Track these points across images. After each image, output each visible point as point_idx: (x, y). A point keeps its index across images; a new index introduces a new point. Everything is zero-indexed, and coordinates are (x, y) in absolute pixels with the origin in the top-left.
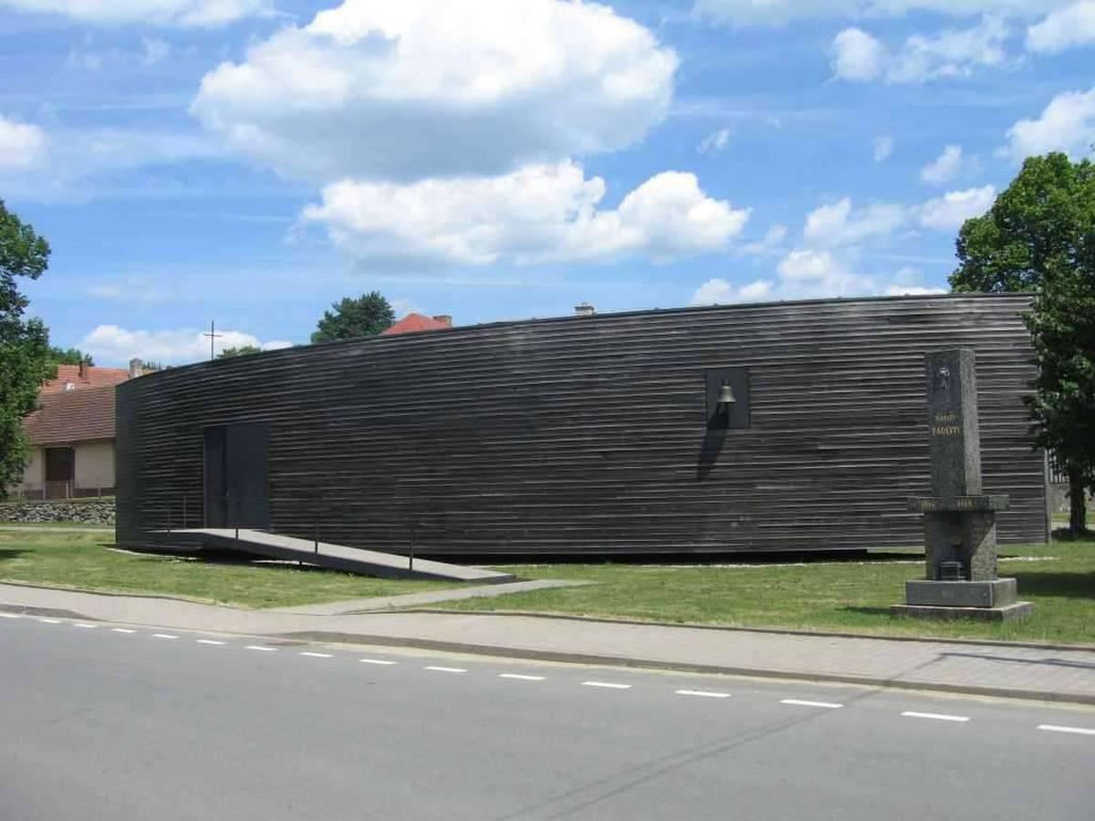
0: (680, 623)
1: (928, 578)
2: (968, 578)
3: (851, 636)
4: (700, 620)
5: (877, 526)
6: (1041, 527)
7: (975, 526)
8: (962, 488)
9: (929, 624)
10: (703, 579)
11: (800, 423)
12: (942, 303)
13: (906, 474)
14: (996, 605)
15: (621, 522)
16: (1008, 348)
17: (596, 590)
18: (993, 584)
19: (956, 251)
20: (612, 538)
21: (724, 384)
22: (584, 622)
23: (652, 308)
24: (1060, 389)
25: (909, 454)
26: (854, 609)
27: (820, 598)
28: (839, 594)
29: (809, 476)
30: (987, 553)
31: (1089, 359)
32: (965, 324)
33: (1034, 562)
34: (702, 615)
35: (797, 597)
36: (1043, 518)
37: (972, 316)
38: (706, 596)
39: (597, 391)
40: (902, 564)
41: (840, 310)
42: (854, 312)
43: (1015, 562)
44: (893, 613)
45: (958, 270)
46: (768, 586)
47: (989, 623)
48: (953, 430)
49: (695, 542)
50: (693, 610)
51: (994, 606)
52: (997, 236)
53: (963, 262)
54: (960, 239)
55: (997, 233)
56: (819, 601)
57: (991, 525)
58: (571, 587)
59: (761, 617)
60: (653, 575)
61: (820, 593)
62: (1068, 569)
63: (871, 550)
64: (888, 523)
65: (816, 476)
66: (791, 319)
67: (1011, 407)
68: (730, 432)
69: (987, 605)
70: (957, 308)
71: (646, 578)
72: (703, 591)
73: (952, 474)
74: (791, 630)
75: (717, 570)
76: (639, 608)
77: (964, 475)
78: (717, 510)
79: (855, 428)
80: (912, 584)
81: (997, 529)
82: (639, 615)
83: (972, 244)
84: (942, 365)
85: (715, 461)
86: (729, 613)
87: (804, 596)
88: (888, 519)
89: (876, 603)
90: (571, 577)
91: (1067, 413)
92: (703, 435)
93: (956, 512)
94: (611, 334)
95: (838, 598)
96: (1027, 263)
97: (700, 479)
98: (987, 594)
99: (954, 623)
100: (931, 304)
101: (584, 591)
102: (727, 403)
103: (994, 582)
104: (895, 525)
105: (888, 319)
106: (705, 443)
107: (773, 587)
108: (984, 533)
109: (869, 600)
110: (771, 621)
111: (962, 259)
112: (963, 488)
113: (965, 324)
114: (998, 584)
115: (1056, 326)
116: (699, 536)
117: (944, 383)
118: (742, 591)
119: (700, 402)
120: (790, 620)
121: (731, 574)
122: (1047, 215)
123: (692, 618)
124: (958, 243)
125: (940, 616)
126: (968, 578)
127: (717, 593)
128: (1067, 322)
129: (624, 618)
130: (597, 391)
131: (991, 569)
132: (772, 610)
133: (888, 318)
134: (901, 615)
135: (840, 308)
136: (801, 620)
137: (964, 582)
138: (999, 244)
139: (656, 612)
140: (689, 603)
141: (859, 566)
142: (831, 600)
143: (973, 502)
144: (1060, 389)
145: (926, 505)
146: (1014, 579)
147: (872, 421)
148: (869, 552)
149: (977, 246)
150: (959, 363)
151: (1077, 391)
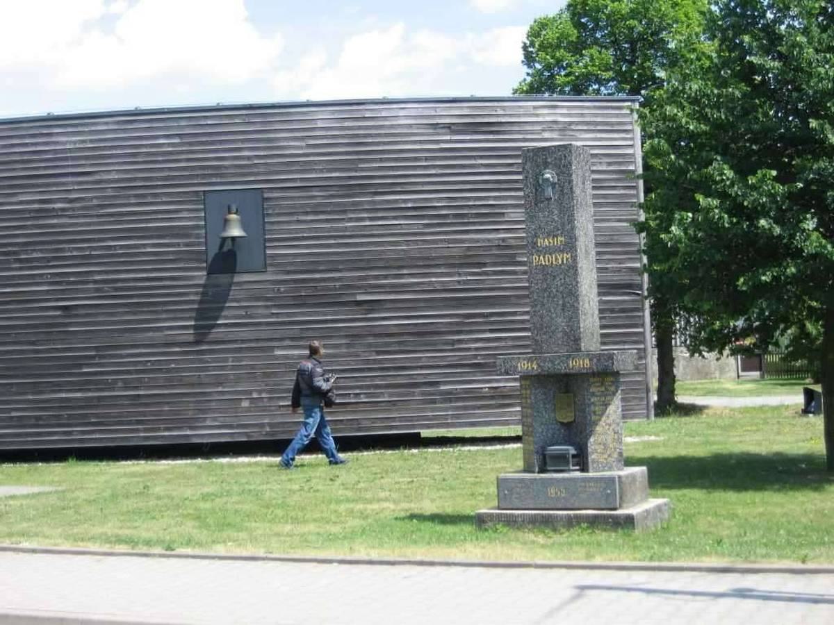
0: (169, 550)
1: (528, 469)
2: (584, 469)
3: (432, 564)
4: (200, 544)
5: (434, 401)
6: (641, 399)
7: (593, 394)
8: (574, 339)
9: (531, 536)
10: (204, 479)
11: (333, 266)
12: (520, 107)
13: (471, 332)
14: (624, 505)
15: (88, 403)
16: (600, 168)
17: (53, 500)
18: (620, 477)
19: (522, 58)
20: (76, 425)
21: (230, 213)
22: (21, 555)
23: (129, 105)
24: (695, 208)
25: (476, 306)
26: (421, 518)
27: (370, 502)
28: (395, 495)
29: (347, 336)
30: (611, 432)
31: (731, 168)
32: (546, 135)
33: (635, 443)
34: (203, 535)
35: (338, 502)
36: (645, 387)
37: (555, 126)
38: (208, 505)
39: (55, 221)
40: (469, 451)
42: (404, 117)
44: (480, 521)
45: (525, 80)
46: (296, 487)
47: (616, 531)
48: (562, 258)
49: (191, 428)
50: (190, 527)
51: (621, 507)
52: (574, 38)
53: (530, 71)
54: (528, 43)
55: (574, 34)
56: (369, 507)
57: (614, 394)
58: (13, 497)
59: (290, 535)
60: (133, 475)
61: (369, 495)
62: (683, 452)
63: (425, 433)
64: (449, 397)
65: (355, 336)
66: (320, 124)
68: (237, 279)
69: (612, 507)
70: (537, 115)
71: (124, 480)
72: (205, 497)
73: (561, 322)
74: (340, 557)
75: (222, 466)
76: (110, 528)
77: (579, 323)
78: (220, 384)
79: (405, 272)
80: (505, 480)
81: (623, 400)
82: (108, 540)
83: (543, 47)
84: (546, 165)
85: (217, 318)
86: (240, 530)
87: (348, 500)
88: (449, 392)
89: (449, 509)
90: (18, 481)
91: (698, 241)
92: (202, 282)
93: (567, 375)
94: (75, 143)
95: (395, 502)
96: (611, 73)
97: (197, 343)
98: (612, 491)
99: (567, 534)
100: (503, 108)
101: (33, 501)
102: (233, 239)
103: (621, 473)
104: (458, 399)
105: (449, 128)
106: (203, 294)
107: (302, 489)
108: (606, 405)
109: (438, 503)
110: (305, 541)
111: (529, 67)
112: (577, 340)
113: (546, 135)
114: (627, 477)
115: (687, 123)
116: (197, 420)
118: (258, 495)
119: (198, 236)
120: (331, 539)
121: (243, 470)
123: (189, 542)
124: (525, 48)
125: (545, 523)
126: (584, 469)
127: (225, 499)
128: (703, 118)
129: (81, 546)
130: (55, 221)
131: (616, 455)
132: (305, 522)
133: (449, 127)
134: (490, 524)
135: (394, 110)
136: (350, 536)
137: (578, 474)
138: (577, 48)
139: (134, 532)
140: (184, 516)
141: (412, 455)
142: (386, 505)
143: (590, 360)
144: (695, 208)
145: (524, 366)
146: (644, 468)
147: (427, 263)
148: (423, 435)
149: (549, 50)
150: (570, 164)
151: (717, 211)
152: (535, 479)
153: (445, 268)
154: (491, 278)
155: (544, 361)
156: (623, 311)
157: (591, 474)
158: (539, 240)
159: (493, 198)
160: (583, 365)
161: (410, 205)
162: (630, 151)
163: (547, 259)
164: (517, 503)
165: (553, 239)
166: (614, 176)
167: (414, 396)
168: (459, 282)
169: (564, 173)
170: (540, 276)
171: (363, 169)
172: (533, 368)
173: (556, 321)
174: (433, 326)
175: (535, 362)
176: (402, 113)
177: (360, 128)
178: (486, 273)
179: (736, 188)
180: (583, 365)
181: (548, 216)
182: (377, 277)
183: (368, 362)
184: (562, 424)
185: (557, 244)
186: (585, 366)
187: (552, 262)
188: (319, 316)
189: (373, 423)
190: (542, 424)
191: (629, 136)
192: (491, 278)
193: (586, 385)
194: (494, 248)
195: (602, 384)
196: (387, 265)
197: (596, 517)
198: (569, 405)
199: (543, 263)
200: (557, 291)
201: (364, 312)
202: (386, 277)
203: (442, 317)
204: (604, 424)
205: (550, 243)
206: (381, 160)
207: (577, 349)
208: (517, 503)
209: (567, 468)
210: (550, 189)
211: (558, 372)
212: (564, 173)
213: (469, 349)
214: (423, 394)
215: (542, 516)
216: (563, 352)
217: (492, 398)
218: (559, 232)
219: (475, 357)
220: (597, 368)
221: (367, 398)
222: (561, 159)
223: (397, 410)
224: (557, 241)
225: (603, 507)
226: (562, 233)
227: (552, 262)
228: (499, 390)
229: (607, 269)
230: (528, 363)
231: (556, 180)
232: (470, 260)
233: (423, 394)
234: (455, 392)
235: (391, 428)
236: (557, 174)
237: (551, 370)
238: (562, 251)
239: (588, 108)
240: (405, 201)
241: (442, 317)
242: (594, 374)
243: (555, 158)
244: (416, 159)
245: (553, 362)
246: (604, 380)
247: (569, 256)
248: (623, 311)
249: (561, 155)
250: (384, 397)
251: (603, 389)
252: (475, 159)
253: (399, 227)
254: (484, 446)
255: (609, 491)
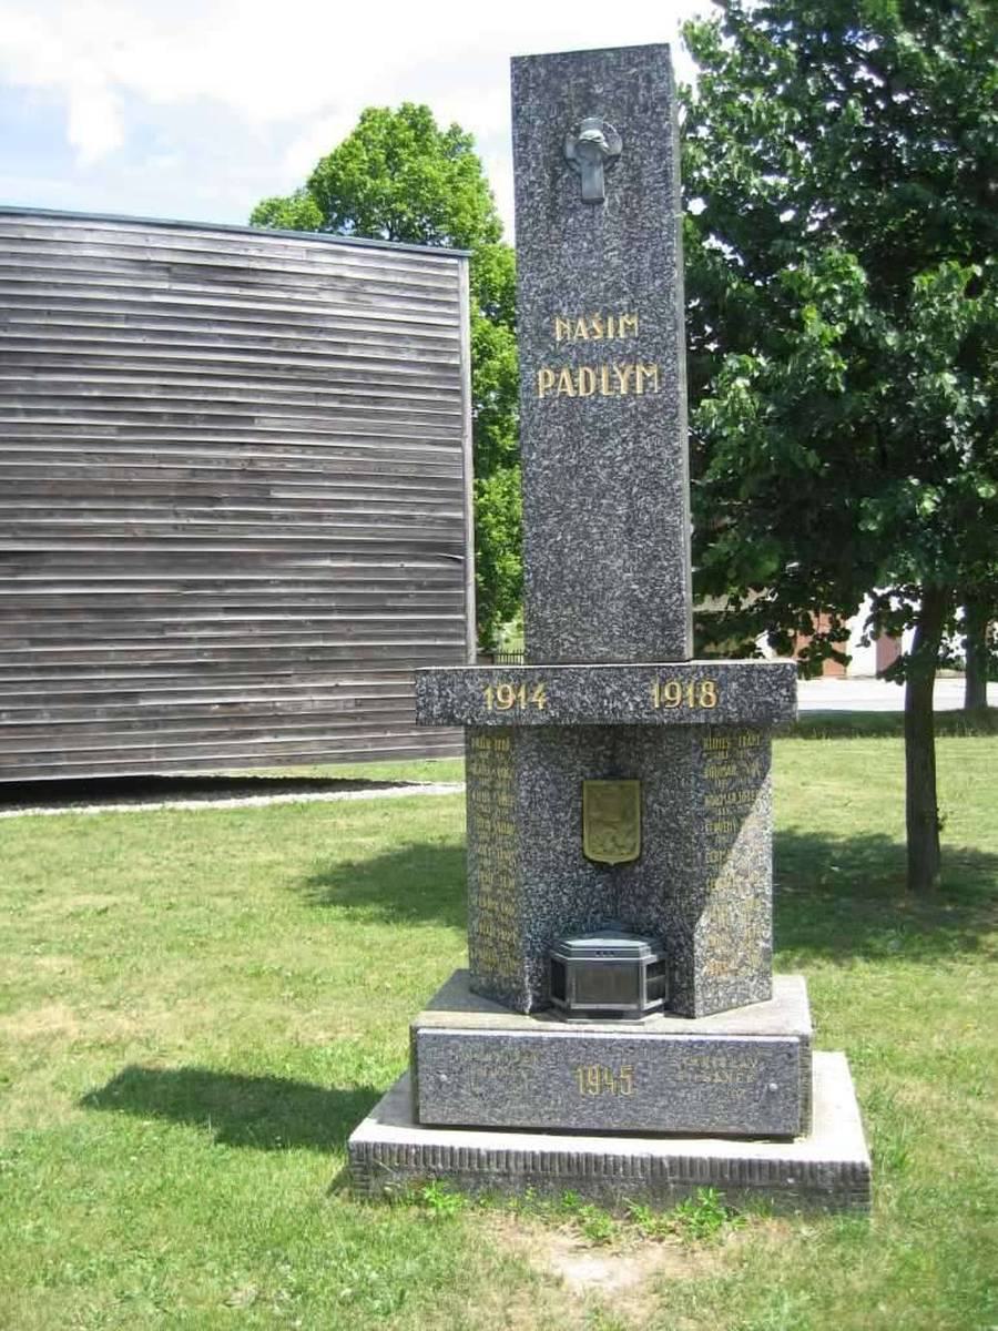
5: (129, 726)
32: (326, 297)
37: (340, 285)
41: (58, 236)
42: (93, 244)
43: (403, 804)
64: (155, 719)
67: (405, 479)
79: (84, 505)
84: (588, 104)
88: (154, 711)
100: (261, 247)
105: (168, 270)
113: (326, 297)
117: (595, 181)
122: (402, 196)
133: (168, 269)
135: (74, 232)
143: (719, 686)
147: (122, 493)
152: (538, 1042)
153: (154, 503)
154: (228, 524)
155: (569, 685)
156: (434, 586)
157: (707, 1026)
158: (558, 323)
159: (234, 391)
160: (696, 701)
161: (96, 393)
162: (453, 335)
163: (581, 380)
164: (475, 1111)
165: (604, 321)
166: (428, 373)
167: (95, 716)
168: (175, 527)
169: (641, 128)
170: (556, 431)
171: (17, 327)
172: (534, 705)
173: (605, 567)
174: (128, 599)
175: (541, 687)
176: (88, 237)
177: (14, 255)
178: (222, 515)
179: (861, 311)
180: (696, 701)
181: (590, 252)
182: (34, 513)
183: (13, 656)
184: (601, 867)
185: (616, 334)
186: (702, 703)
187: (597, 391)
188: (140, 770)
189: (23, 761)
190: (546, 869)
191: (452, 312)
192: (228, 524)
193: (691, 760)
194: (235, 474)
195: (732, 758)
196: (55, 492)
197: (747, 1167)
198: (626, 816)
199: (571, 393)
200: (611, 476)
201: (10, 571)
202: (50, 513)
203: (147, 584)
204: (733, 871)
205: (592, 332)
206: (50, 313)
207: (669, 651)
208: (475, 1111)
209: (634, 1007)
210: (598, 173)
211: (611, 719)
212: (641, 128)
213: (188, 640)
214: (110, 712)
215: (568, 1161)
216: (625, 656)
217: (225, 721)
218: (624, 302)
219: (199, 652)
220: (740, 712)
221: (12, 718)
222: (635, 89)
223: (65, 739)
224: (617, 328)
225: (752, 1129)
226: (632, 304)
227: (597, 391)
228: (235, 709)
229: (411, 517)
230: (517, 691)
231: (618, 147)
232: (193, 492)
233: (110, 712)
234: (163, 710)
235: (54, 769)
236: (622, 132)
237: (593, 716)
238: (632, 359)
239: (393, 261)
240: (89, 385)
241: (147, 584)
242: (711, 730)
243: (618, 86)
244: (110, 317)
245: (596, 688)
246: (735, 743)
247: (653, 371)
248: (434, 586)
249: (635, 76)
250: (42, 718)
251: (732, 770)
252: (209, 325)
253: (76, 429)
254: (210, 800)
255: (774, 1086)
